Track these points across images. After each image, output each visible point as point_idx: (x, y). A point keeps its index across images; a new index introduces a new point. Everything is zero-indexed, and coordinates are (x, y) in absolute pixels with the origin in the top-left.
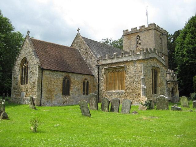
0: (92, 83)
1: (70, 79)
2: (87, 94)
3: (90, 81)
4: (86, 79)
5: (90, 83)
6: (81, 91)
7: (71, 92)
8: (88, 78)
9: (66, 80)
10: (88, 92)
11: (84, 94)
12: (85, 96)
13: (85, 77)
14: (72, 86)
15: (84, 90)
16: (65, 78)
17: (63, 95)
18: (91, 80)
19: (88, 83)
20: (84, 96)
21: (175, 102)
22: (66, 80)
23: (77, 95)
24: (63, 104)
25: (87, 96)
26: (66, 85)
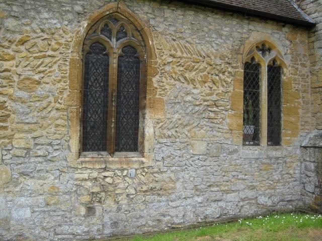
0: (305, 71)
1: (144, 40)
2: (275, 139)
3: (287, 61)
4: (264, 48)
5: (287, 74)
6: (232, 118)
7: (149, 127)
8: (281, 41)
9: (115, 45)
10: (279, 125)
11: (253, 139)
12: (263, 149)
13: (258, 33)
14: (163, 85)
15: (251, 116)
16: (106, 30)
17: (87, 145)
18: (295, 58)
19: (275, 71)
20: (252, 151)
21: (247, 71)
22: (115, 45)
23: (200, 147)
24: (83, 210)
25: (278, 154)
26: (114, 62)
